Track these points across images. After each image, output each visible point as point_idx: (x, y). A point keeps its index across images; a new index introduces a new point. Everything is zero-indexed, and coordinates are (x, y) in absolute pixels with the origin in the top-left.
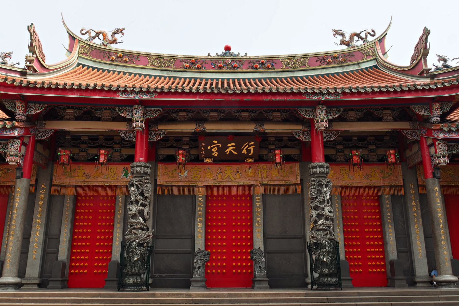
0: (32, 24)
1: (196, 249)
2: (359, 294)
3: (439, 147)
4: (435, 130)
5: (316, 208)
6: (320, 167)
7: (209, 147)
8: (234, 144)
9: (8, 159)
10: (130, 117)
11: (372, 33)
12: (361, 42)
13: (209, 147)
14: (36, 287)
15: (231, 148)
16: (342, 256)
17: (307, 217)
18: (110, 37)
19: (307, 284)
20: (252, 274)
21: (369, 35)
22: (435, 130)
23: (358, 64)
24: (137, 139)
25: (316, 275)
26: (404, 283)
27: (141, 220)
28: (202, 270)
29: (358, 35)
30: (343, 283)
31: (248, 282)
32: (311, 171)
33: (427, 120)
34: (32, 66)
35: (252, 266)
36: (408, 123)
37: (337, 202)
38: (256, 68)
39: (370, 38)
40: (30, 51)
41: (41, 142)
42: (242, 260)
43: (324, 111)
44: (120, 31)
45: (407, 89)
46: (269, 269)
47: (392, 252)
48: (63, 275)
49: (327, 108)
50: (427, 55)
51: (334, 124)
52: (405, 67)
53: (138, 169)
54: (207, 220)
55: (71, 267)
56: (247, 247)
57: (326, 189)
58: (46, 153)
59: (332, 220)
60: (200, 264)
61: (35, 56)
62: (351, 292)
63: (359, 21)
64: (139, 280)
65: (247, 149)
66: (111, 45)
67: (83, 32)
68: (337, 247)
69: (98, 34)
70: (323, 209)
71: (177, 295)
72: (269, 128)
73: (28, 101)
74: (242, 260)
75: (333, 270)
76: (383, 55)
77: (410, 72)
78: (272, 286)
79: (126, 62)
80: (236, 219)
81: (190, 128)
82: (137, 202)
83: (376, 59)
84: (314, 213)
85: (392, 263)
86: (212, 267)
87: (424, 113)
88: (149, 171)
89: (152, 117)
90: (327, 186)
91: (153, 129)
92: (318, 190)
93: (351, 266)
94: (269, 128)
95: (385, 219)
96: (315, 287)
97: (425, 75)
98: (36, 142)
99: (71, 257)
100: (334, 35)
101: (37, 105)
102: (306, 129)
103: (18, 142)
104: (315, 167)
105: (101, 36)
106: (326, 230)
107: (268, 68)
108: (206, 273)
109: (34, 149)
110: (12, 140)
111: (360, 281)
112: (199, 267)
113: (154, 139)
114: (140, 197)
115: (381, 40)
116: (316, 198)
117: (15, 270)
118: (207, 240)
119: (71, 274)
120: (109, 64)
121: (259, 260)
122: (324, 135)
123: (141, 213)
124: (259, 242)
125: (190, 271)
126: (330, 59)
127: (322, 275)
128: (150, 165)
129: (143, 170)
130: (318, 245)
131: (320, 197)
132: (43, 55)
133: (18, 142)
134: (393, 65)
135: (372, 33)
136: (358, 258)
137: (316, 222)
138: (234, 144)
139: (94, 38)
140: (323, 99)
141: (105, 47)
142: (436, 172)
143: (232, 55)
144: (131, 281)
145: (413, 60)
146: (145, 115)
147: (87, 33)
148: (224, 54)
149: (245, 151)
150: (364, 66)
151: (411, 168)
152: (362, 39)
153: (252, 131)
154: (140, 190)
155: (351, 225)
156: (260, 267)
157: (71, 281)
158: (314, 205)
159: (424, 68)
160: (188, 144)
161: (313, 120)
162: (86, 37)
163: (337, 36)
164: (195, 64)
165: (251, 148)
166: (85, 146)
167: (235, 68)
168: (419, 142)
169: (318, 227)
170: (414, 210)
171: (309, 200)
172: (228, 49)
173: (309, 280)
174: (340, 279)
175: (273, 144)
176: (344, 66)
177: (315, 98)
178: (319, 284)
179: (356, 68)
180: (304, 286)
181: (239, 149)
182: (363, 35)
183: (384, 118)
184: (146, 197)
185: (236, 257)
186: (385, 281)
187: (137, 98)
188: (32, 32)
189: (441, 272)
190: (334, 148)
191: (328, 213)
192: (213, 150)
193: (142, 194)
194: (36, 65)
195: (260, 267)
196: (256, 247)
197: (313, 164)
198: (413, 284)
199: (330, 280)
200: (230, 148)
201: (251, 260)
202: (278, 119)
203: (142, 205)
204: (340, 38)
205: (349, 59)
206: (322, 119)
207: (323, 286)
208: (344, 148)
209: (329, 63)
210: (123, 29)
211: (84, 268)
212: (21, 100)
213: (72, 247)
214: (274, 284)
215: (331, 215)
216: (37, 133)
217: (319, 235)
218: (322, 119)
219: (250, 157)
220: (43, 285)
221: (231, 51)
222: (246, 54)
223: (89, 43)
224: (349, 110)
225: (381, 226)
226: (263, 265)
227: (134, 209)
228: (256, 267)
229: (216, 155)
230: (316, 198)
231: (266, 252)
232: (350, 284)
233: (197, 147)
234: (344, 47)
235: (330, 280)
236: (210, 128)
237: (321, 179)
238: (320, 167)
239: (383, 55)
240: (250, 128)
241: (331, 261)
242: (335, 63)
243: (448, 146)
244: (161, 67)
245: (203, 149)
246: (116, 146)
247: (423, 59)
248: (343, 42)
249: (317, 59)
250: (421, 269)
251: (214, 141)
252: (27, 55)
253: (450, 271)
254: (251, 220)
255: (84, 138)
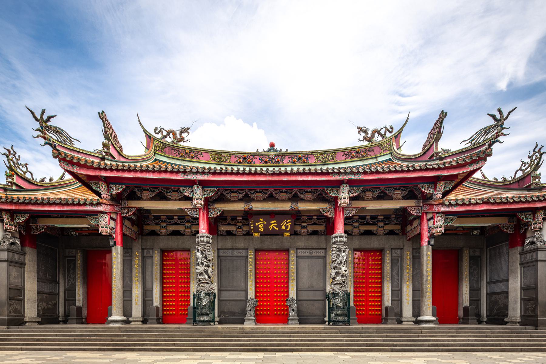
0: (103, 111)
1: (249, 298)
2: (363, 328)
3: (437, 219)
4: (436, 205)
5: (335, 268)
6: (340, 237)
7: (257, 224)
8: (275, 221)
9: (100, 230)
10: (191, 196)
11: (391, 130)
12: (380, 138)
13: (257, 224)
14: (141, 323)
15: (273, 225)
16: (352, 304)
17: (328, 275)
18: (178, 136)
19: (326, 322)
20: (288, 315)
21: (387, 132)
22: (436, 205)
23: (376, 158)
24: (200, 215)
25: (333, 315)
26: (394, 321)
27: (206, 277)
28: (252, 312)
29: (378, 132)
30: (351, 321)
31: (284, 319)
32: (333, 240)
33: (431, 197)
34: (109, 153)
35: (287, 310)
36: (414, 201)
37: (351, 265)
38: (294, 162)
39: (388, 135)
40: (106, 138)
41: (129, 219)
42: (280, 306)
43: (347, 190)
44: (185, 130)
45: (419, 168)
46: (299, 312)
47: (388, 301)
48: (157, 315)
49: (350, 187)
50: (439, 140)
51: (354, 202)
52: (416, 155)
53: (202, 239)
54: (256, 279)
55: (164, 310)
56: (284, 297)
57: (343, 254)
58: (135, 229)
59: (346, 277)
60: (251, 308)
61: (110, 143)
62: (356, 326)
63: (381, 117)
64: (207, 318)
65: (285, 226)
66: (180, 143)
67: (157, 132)
68: (348, 296)
69: (168, 133)
70: (340, 269)
71: (233, 327)
72: (302, 206)
73: (109, 181)
74: (280, 306)
75: (344, 312)
76: (398, 149)
77: (420, 159)
78: (301, 322)
79: (193, 158)
80: (277, 278)
81: (240, 206)
82: (202, 263)
83: (391, 153)
84: (333, 272)
85: (387, 309)
86: (260, 310)
87: (428, 191)
88: (210, 241)
89: (209, 196)
90: (344, 251)
91: (212, 207)
92: (338, 255)
93: (357, 310)
94: (302, 206)
95: (385, 277)
96: (331, 324)
97: (435, 158)
98: (123, 218)
99: (163, 303)
100: (359, 133)
101: (117, 186)
102: (331, 207)
103: (107, 217)
104: (337, 237)
105: (171, 135)
106: (341, 284)
107: (304, 162)
108: (256, 314)
109: (122, 225)
110: (100, 215)
111: (362, 320)
112: (250, 310)
113: (213, 215)
114: (204, 259)
115: (397, 136)
116: (335, 261)
117: (121, 311)
118: (256, 292)
119: (163, 314)
120: (179, 160)
121: (293, 305)
122: (345, 211)
123: (206, 272)
124: (292, 293)
125: (244, 312)
126: (354, 153)
127: (337, 315)
128: (211, 236)
129: (205, 239)
130: (335, 295)
131: (339, 260)
132: (120, 144)
133: (107, 217)
134: (406, 156)
135: (391, 130)
136: (362, 305)
137: (334, 278)
138: (275, 221)
139: (166, 137)
140: (347, 178)
141: (175, 145)
142: (431, 240)
143: (276, 151)
144: (202, 318)
145: (424, 146)
146: (202, 194)
147: (159, 132)
148: (269, 150)
149: (283, 227)
150: (380, 159)
151: (409, 240)
152: (382, 135)
153: (289, 209)
154: (204, 254)
155: (359, 282)
156: (293, 310)
157: (163, 319)
158: (333, 265)
159: (435, 151)
160: (241, 222)
161: (337, 197)
162: (159, 136)
163: (361, 133)
164: (245, 158)
165: (289, 224)
166: (164, 224)
167: (278, 162)
168: (420, 218)
169: (336, 282)
170: (407, 271)
171: (331, 262)
172: (272, 145)
173: (327, 319)
174: (349, 318)
175: (305, 222)
176: (365, 160)
177: (340, 178)
178: (333, 321)
179: (374, 161)
180: (324, 322)
181: (279, 226)
182: (382, 132)
183: (395, 197)
184: (209, 260)
185: (277, 304)
186: (378, 319)
187: (195, 178)
188: (104, 120)
189: (40, 282)
190: (351, 225)
191: (344, 272)
192: (260, 226)
193: (206, 257)
194: (112, 151)
195: (293, 310)
196: (291, 296)
197: (335, 235)
198: (400, 322)
199: (341, 319)
200: (273, 225)
201: (287, 306)
202: (309, 199)
203: (206, 266)
204: (363, 134)
205: (369, 153)
206: (344, 195)
207: (336, 323)
208: (359, 224)
209: (352, 157)
210: (189, 129)
211: (172, 310)
212: (103, 181)
213: (163, 296)
214: (302, 320)
215: (346, 273)
216: (123, 211)
217: (336, 288)
218: (344, 195)
219: (288, 232)
220: (145, 321)
221: (275, 148)
222: (287, 150)
223: (162, 141)
224: (367, 191)
225: (382, 283)
226: (295, 309)
227: (201, 269)
228: (290, 310)
229: (262, 231)
230: (335, 261)
231: (298, 300)
232: (356, 321)
233: (248, 225)
234: (366, 143)
235: (341, 319)
236: (256, 206)
237: (340, 246)
238: (340, 237)
239: (398, 149)
240: (287, 206)
241: (344, 306)
242: (357, 157)
243: (445, 219)
244: (220, 161)
245: (252, 225)
246: (187, 224)
247: (435, 144)
248: (365, 139)
249: (343, 153)
250: (408, 311)
251: (261, 220)
252: (103, 142)
253: (431, 314)
254: (288, 279)
255: (163, 218)
